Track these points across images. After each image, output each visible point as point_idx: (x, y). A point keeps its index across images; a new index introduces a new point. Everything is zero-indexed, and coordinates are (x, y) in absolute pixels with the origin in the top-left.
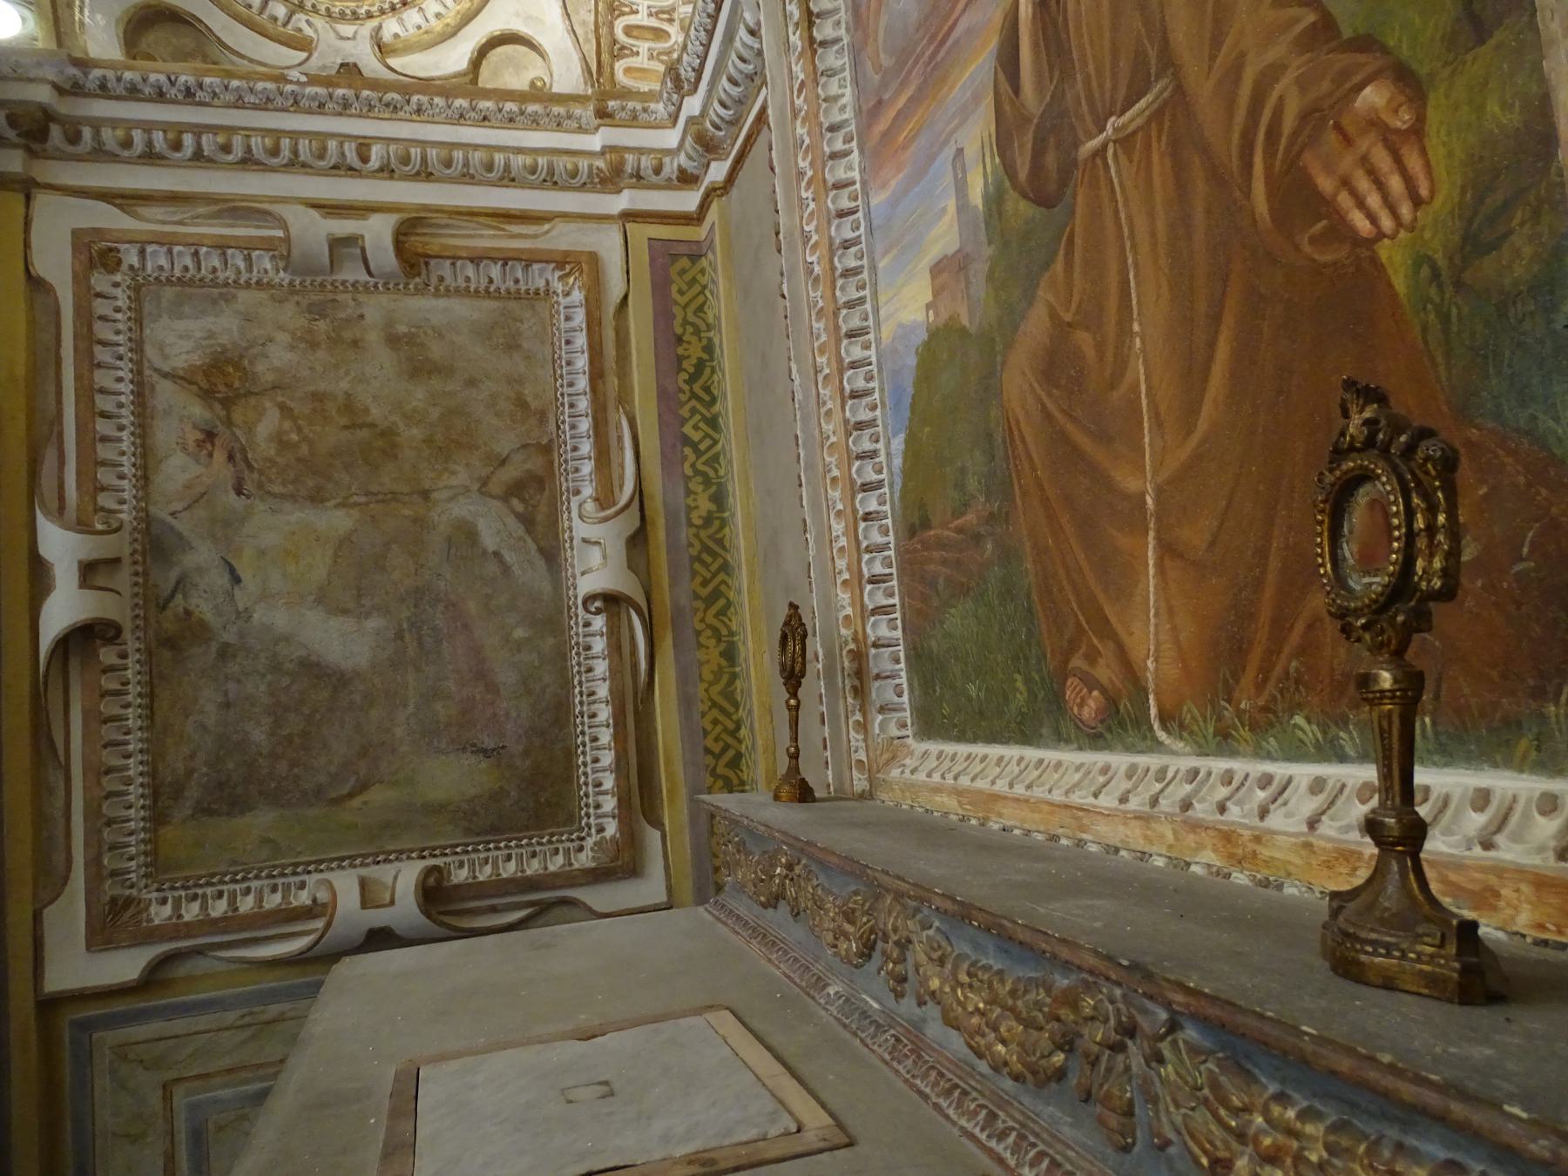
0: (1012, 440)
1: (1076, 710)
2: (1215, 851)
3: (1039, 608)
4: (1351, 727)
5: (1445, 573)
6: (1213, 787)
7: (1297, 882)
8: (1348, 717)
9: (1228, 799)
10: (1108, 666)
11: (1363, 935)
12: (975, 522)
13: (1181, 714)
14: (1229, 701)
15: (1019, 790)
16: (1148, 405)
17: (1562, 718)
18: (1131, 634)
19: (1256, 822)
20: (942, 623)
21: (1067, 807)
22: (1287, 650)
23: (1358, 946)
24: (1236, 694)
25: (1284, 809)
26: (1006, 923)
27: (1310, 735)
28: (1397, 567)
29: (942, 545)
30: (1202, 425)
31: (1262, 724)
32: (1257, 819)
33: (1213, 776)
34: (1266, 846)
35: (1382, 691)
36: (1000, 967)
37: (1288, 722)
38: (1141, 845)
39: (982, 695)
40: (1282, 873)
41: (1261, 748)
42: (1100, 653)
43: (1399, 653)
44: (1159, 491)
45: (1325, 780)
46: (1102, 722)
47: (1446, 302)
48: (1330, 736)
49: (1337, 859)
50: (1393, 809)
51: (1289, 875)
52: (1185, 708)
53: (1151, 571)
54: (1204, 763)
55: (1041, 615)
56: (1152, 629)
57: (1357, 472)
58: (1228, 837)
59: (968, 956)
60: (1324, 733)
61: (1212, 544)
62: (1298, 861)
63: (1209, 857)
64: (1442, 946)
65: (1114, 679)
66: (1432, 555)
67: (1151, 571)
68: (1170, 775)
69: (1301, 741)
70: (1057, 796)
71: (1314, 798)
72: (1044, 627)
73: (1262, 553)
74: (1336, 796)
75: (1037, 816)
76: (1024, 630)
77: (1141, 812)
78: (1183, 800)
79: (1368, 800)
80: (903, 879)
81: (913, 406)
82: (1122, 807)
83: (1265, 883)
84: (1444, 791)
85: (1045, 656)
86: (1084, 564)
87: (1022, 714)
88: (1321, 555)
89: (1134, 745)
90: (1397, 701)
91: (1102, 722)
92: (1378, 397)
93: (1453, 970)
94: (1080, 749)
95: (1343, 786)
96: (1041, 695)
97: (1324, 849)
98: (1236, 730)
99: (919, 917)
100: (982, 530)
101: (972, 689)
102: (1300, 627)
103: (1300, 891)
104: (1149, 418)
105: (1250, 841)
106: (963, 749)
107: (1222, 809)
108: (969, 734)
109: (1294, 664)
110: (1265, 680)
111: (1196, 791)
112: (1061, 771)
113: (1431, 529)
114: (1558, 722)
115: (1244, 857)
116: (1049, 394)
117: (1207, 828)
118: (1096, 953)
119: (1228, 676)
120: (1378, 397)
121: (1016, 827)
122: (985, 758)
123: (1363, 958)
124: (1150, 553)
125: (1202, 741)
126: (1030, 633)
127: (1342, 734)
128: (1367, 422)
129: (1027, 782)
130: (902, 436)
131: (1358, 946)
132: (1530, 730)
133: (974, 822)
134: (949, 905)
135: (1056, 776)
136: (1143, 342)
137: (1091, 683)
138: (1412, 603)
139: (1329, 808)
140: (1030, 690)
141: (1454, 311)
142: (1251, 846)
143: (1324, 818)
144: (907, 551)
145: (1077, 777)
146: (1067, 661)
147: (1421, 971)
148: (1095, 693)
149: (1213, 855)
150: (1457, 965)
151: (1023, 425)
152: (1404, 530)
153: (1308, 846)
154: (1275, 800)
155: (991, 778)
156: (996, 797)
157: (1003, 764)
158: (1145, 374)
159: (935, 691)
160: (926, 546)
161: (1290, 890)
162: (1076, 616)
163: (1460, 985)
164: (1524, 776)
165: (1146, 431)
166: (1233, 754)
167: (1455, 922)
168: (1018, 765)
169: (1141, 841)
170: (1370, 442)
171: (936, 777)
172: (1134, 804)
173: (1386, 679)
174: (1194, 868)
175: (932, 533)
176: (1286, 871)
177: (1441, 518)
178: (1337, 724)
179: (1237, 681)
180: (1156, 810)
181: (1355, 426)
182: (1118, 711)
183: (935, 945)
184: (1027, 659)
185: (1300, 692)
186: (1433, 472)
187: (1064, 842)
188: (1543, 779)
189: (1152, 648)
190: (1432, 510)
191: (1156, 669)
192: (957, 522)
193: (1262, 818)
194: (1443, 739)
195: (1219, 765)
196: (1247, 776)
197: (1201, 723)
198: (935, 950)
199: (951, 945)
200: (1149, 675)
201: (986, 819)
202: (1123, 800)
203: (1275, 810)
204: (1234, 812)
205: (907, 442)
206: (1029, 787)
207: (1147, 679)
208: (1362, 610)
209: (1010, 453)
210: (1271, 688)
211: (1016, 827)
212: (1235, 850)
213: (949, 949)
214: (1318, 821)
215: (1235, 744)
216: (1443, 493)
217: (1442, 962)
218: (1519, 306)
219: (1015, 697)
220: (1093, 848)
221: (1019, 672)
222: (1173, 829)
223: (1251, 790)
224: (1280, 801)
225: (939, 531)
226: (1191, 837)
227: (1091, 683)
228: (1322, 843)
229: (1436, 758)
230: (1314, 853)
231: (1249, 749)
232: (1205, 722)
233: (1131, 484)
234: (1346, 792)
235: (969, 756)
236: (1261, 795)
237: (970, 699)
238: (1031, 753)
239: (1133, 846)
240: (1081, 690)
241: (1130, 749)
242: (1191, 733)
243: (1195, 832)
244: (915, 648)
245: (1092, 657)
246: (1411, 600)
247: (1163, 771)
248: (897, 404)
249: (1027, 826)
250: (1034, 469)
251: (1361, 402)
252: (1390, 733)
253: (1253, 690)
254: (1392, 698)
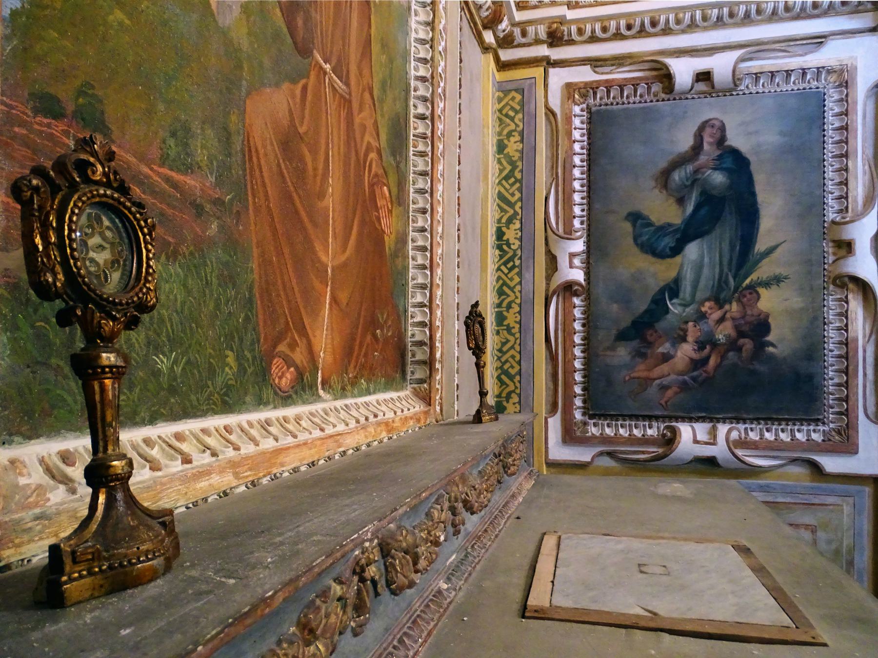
73: (359, 314)
221: (232, 350)
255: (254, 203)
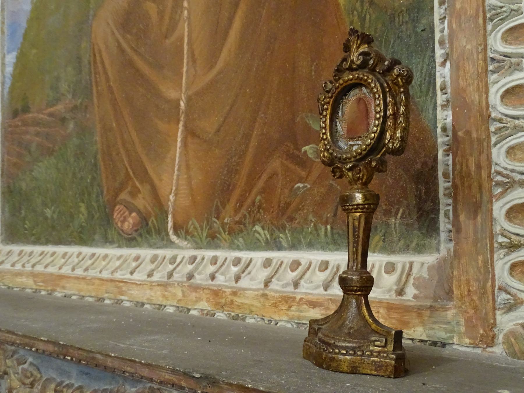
0: (95, 62)
1: (119, 224)
2: (208, 301)
3: (102, 164)
4: (287, 231)
5: (403, 139)
6: (205, 266)
7: (256, 316)
8: (285, 227)
9: (216, 272)
10: (144, 198)
11: (340, 344)
12: (63, 111)
13: (187, 227)
14: (218, 218)
15: (79, 272)
16: (188, 50)
17: (397, 225)
18: (161, 180)
19: (233, 284)
20: (31, 171)
21: (112, 281)
22: (255, 190)
23: (337, 351)
24: (222, 216)
25: (249, 276)
26: (99, 356)
27: (263, 236)
28: (376, 135)
29: (37, 123)
30: (220, 64)
31: (236, 230)
32: (234, 282)
33: (205, 260)
34: (239, 297)
35: (358, 205)
36: (80, 384)
37: (251, 230)
38: (160, 300)
39: (55, 216)
40: (248, 311)
41: (234, 244)
42: (139, 190)
43: (365, 184)
44: (189, 99)
45: (271, 260)
46: (136, 231)
47: (364, 11)
48: (274, 236)
49: (280, 302)
50: (356, 270)
51: (251, 312)
52: (190, 222)
53: (179, 144)
54: (200, 253)
55: (103, 168)
56: (175, 177)
57: (353, 81)
58: (216, 293)
59: (54, 379)
60: (272, 235)
61: (218, 130)
62: (258, 305)
63: (204, 305)
64: (385, 346)
65: (147, 206)
66: (395, 129)
67: (179, 144)
68: (178, 260)
69: (258, 239)
70: (105, 275)
71: (265, 270)
72: (104, 175)
73: (247, 137)
74: (278, 268)
75: (90, 287)
76: (90, 177)
77: (162, 281)
78: (188, 274)
79: (296, 270)
80: (13, 333)
81: (25, 36)
82: (149, 279)
83: (236, 318)
84: (337, 263)
85: (102, 192)
86: (136, 140)
87: (81, 227)
88: (325, 128)
89: (155, 244)
90: (365, 210)
91: (136, 231)
92: (367, 39)
93: (391, 359)
94: (119, 247)
95: (282, 263)
96: (97, 216)
97: (274, 297)
98: (220, 234)
99: (15, 357)
100: (68, 116)
101: (48, 212)
102: (265, 177)
103: (256, 320)
104: (188, 57)
105: (230, 294)
106: (38, 249)
107: (213, 277)
108: (43, 240)
109: (259, 198)
110: (241, 206)
111: (196, 269)
112: (107, 260)
113: (395, 115)
114: (395, 227)
115: (226, 304)
116: (124, 37)
117: (204, 289)
118: (174, 371)
119: (219, 204)
120: (367, 39)
121: (74, 295)
122: (54, 254)
123: (341, 357)
124: (179, 134)
125: (199, 241)
126: (94, 178)
127: (281, 235)
128: (362, 54)
129: (84, 267)
130: (15, 54)
131: (337, 351)
132: (381, 231)
133: (43, 293)
134: (50, 348)
135: (104, 263)
136: (189, 13)
137: (131, 208)
138: (379, 156)
139: (275, 274)
140: (89, 212)
141: (368, 16)
142: (230, 297)
143: (273, 280)
144: (10, 126)
145: (118, 263)
146: (116, 195)
147: (373, 361)
148: (134, 214)
149: (206, 304)
150: (394, 356)
151: (104, 55)
152: (382, 114)
153: (264, 295)
154: (243, 272)
155: (58, 266)
156: (62, 277)
157: (67, 257)
158: (188, 32)
159: (21, 213)
160: (25, 124)
161: (250, 320)
162: (127, 169)
163: (395, 366)
164: (376, 254)
165: (185, 64)
166: (217, 247)
167: (393, 332)
168: (78, 257)
169: (161, 299)
170: (363, 66)
171: (18, 267)
172: (156, 277)
173: (359, 198)
174: (192, 312)
175: (30, 115)
176: (250, 309)
177: (402, 109)
178: (279, 230)
179: (224, 208)
180: (171, 280)
181: (355, 57)
182: (147, 224)
183: (29, 374)
184: (89, 194)
185: (260, 213)
186: (401, 83)
187: (107, 302)
188: (385, 255)
189: (174, 188)
190: (396, 105)
191: (175, 200)
192: (52, 110)
193: (237, 282)
194: (336, 236)
195: (209, 254)
196: (226, 259)
197: (200, 231)
198: (28, 378)
199: (40, 373)
200: (170, 204)
201: (54, 290)
202: (150, 275)
203: (244, 277)
204: (220, 279)
205: (18, 58)
206: (86, 270)
207: (168, 206)
208: (350, 159)
209: (93, 70)
210: (243, 211)
211: (74, 295)
212: (220, 301)
213: (39, 376)
214: (270, 282)
215: (219, 242)
216: (404, 95)
217: (385, 355)
218: (401, 18)
219: (78, 217)
220: (127, 304)
221: (83, 202)
222: (182, 290)
223: (228, 266)
224: (246, 272)
225: (36, 115)
226: (194, 294)
227: (131, 208)
228: (273, 294)
229: (331, 247)
230: (268, 299)
231: (227, 245)
232: (202, 230)
233: (172, 94)
234: (284, 266)
235: (42, 253)
236: (235, 270)
237: (46, 218)
238: (87, 250)
239: (154, 302)
240: (124, 213)
241: (151, 246)
242: (193, 236)
243: (196, 292)
244: (9, 187)
245: (134, 193)
246: (378, 154)
247: (174, 258)
248: (13, 34)
249: (82, 294)
250: (108, 80)
251: (359, 42)
252: (359, 229)
253: (233, 213)
254: (362, 209)
255: (98, 90)
